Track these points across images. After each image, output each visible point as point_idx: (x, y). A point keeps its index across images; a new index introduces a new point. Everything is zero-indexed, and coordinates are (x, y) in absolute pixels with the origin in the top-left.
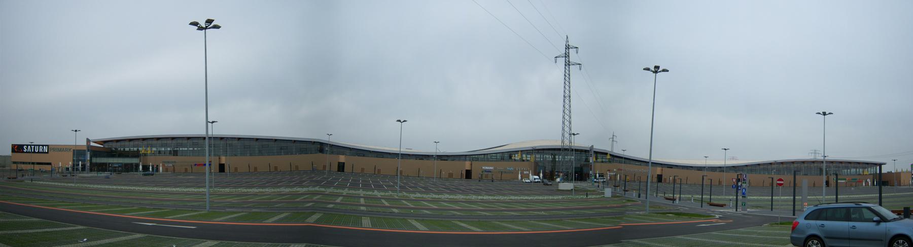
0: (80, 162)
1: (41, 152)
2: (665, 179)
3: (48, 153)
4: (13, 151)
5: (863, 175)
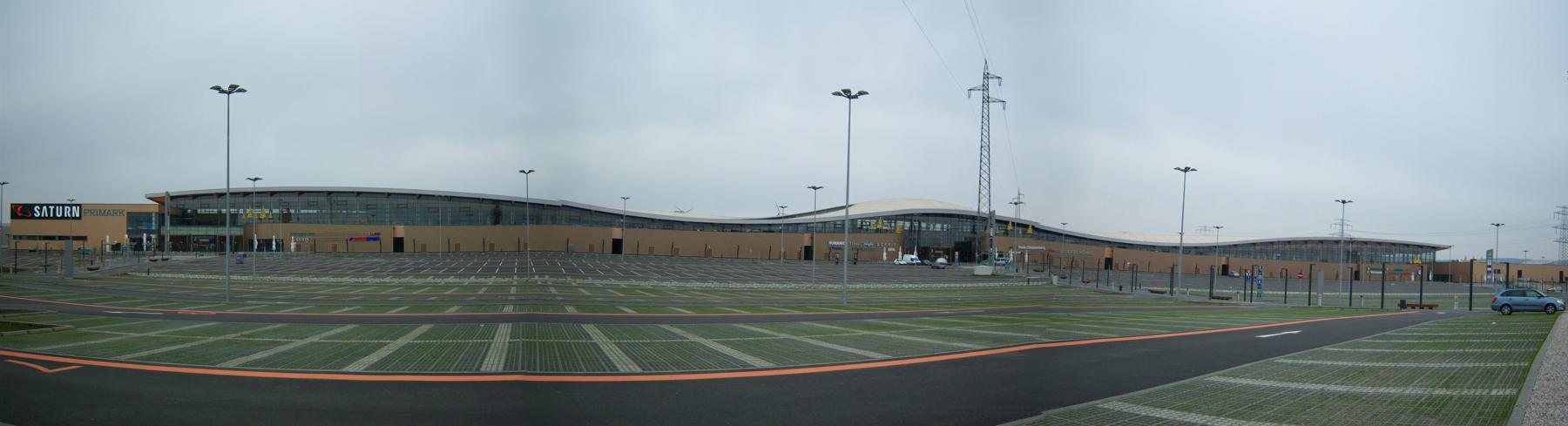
0: (145, 235)
1: (68, 218)
2: (1117, 265)
3: (80, 218)
4: (14, 215)
5: (1413, 263)
